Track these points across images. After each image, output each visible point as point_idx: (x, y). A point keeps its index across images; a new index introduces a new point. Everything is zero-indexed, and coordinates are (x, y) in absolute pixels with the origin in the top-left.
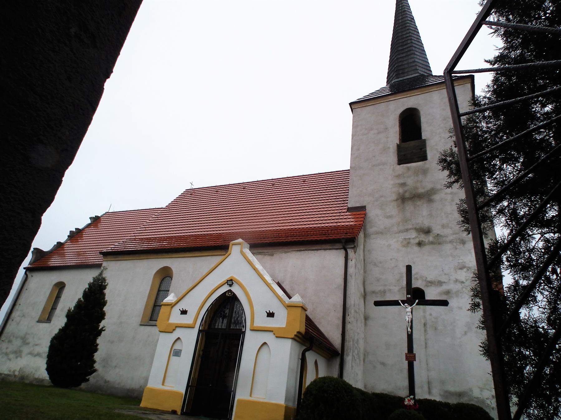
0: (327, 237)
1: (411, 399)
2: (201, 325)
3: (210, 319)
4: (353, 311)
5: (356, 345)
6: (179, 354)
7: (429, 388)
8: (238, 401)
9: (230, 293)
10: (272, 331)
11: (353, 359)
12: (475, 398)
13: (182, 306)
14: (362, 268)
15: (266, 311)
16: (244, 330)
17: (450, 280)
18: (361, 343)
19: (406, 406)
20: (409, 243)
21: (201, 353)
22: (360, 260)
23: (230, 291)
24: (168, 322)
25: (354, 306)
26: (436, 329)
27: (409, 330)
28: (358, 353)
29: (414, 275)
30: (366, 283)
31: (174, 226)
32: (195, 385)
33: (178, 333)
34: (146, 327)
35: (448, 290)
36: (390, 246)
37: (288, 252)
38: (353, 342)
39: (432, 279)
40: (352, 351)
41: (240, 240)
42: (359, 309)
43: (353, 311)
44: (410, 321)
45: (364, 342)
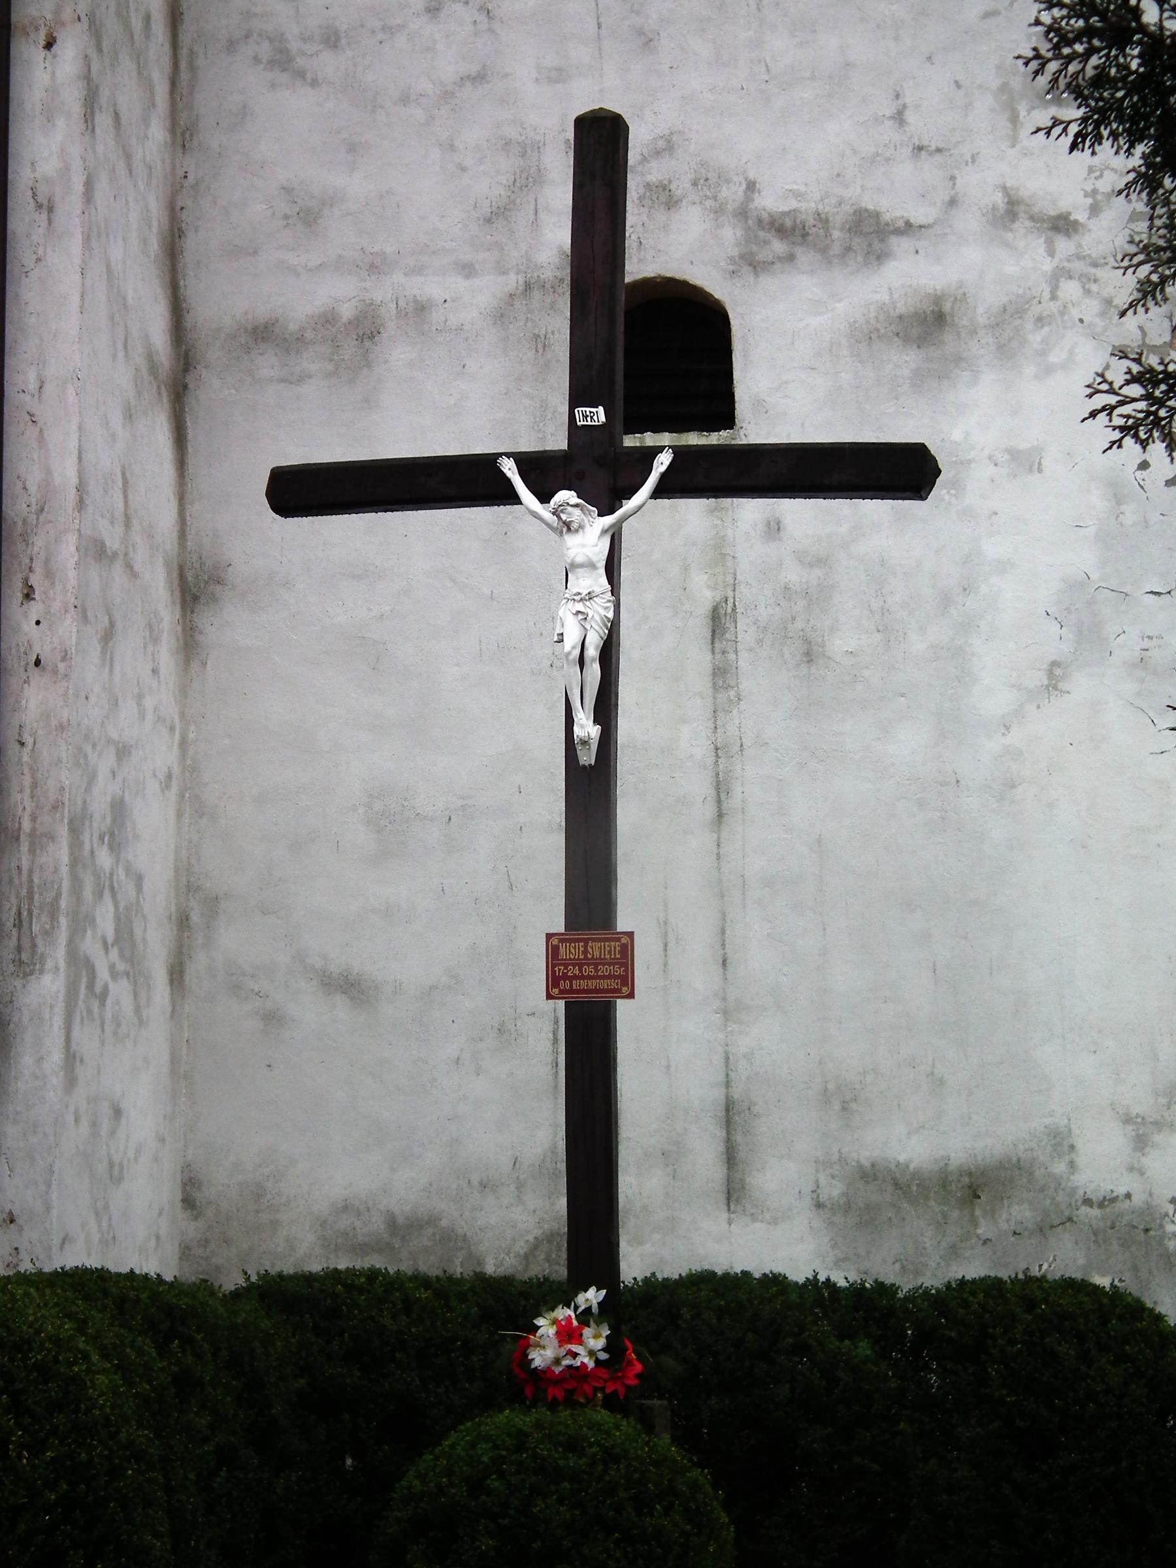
1: (585, 1316)
4: (68, 552)
5: (104, 859)
7: (731, 1157)
11: (83, 991)
12: (1088, 1202)
17: (953, 202)
22: (137, 23)
25: (81, 504)
26: (811, 654)
27: (587, 728)
29: (644, 160)
30: (191, 244)
35: (938, 299)
38: (76, 843)
39: (797, 195)
40: (63, 921)
42: (128, 524)
44: (592, 652)
45: (179, 815)
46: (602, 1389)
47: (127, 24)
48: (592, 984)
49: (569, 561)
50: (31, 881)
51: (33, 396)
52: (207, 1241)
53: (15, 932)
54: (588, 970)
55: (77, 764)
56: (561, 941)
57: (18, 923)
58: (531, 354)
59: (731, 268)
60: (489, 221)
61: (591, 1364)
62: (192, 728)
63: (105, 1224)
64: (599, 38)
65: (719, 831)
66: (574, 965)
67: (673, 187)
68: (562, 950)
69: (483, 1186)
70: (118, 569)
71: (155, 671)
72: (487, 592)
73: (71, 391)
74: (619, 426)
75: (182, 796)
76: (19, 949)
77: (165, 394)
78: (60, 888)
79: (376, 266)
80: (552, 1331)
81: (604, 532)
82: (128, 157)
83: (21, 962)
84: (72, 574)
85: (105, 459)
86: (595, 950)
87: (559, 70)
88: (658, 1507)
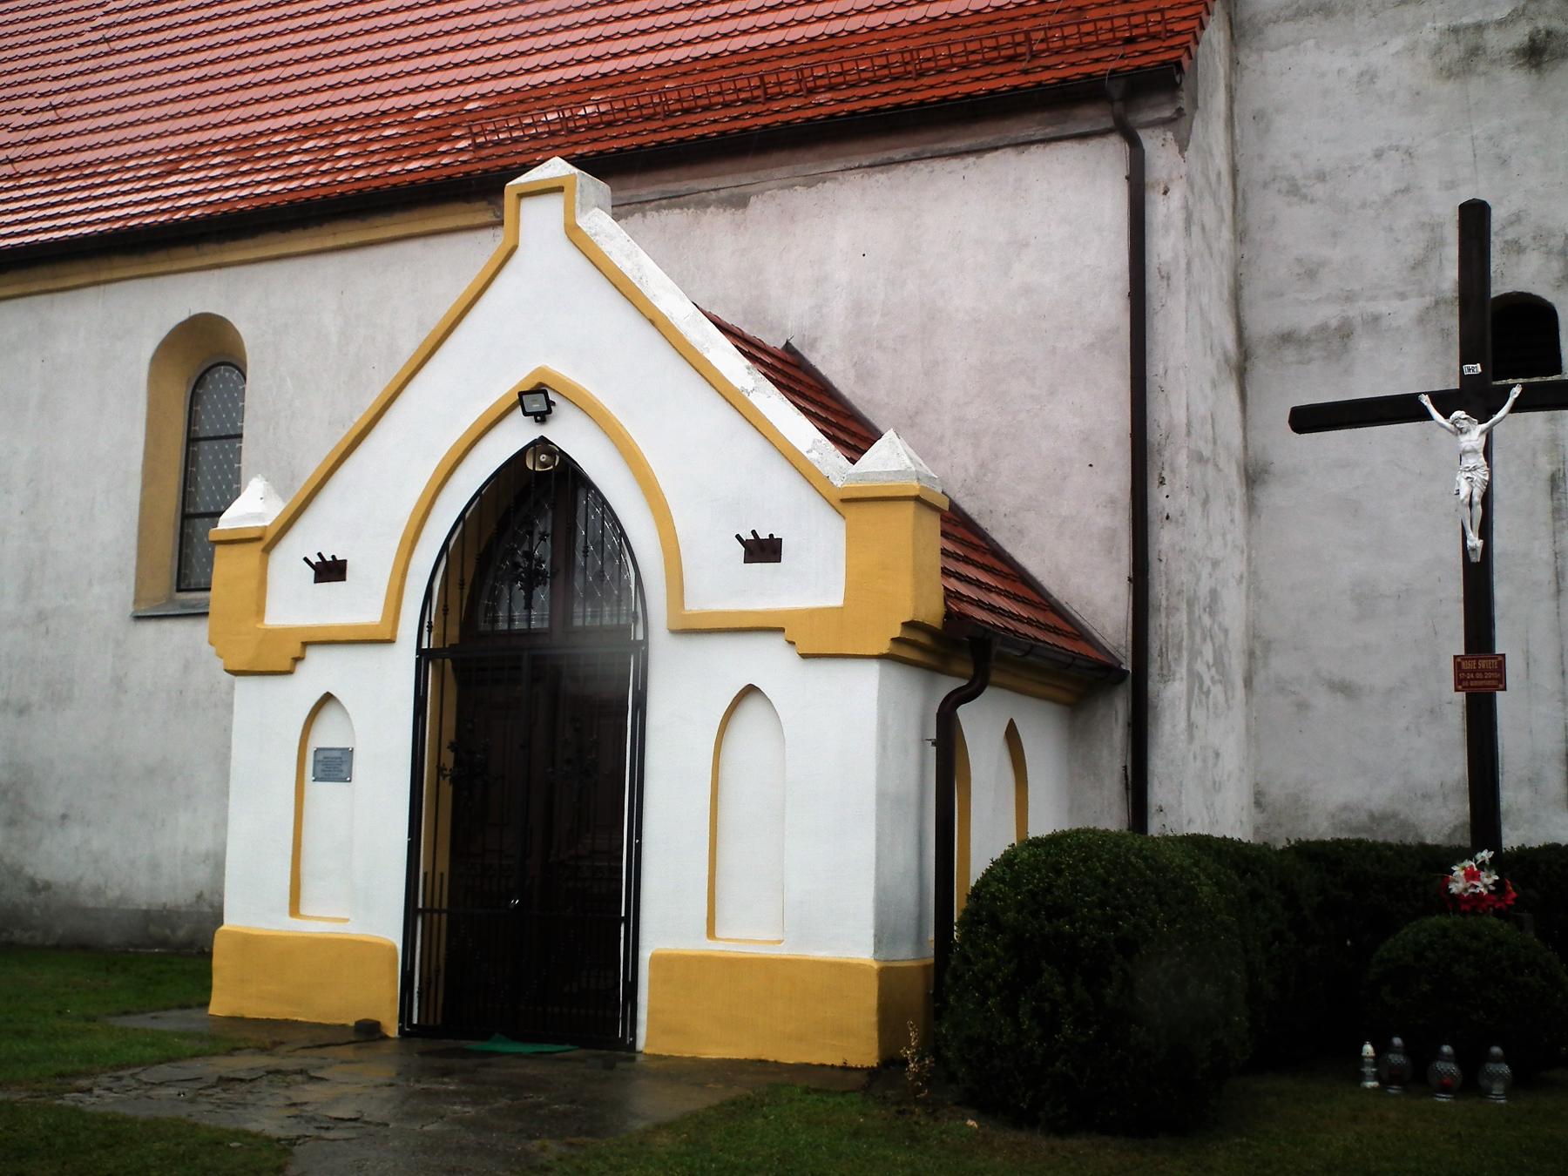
0: (1025, 72)
1: (1482, 866)
2: (426, 629)
3: (467, 591)
4: (1182, 459)
5: (1207, 620)
6: (344, 768)
8: (656, 960)
9: (543, 458)
10: (782, 630)
13: (311, 539)
14: (1222, 220)
15: (738, 537)
16: (640, 637)
18: (1234, 609)
19: (1457, 898)
20: (1475, 52)
21: (449, 759)
22: (1213, 178)
23: (542, 444)
24: (259, 626)
25: (1189, 433)
27: (1475, 541)
28: (1215, 659)
30: (1246, 293)
31: (199, 80)
32: (445, 906)
33: (320, 671)
34: (167, 625)
36: (1372, 81)
37: (823, 178)
38: (1190, 612)
40: (1185, 654)
41: (556, 168)
42: (1215, 443)
43: (1182, 459)
44: (1477, 499)
45: (1248, 597)
46: (1493, 906)
47: (1207, 178)
48: (1481, 683)
49: (1462, 449)
50: (1167, 632)
51: (1161, 377)
52: (1269, 824)
53: (1159, 658)
54: (1479, 675)
55: (1190, 570)
56: (1465, 659)
57: (1161, 655)
58: (1440, 340)
59: (1558, 284)
60: (1413, 268)
61: (1485, 892)
62: (1253, 551)
63: (1211, 813)
64: (1475, 162)
65: (1558, 600)
66: (1470, 673)
67: (1521, 241)
68: (1463, 663)
69: (1424, 796)
70: (1210, 467)
71: (1232, 521)
72: (1418, 471)
73: (1182, 373)
74: (1490, 375)
75: (1249, 587)
76: (1162, 668)
77: (1234, 374)
78: (1182, 636)
79: (1350, 298)
80: (1462, 873)
81: (1482, 432)
82: (1210, 247)
83: (1163, 675)
84: (1185, 470)
85: (1201, 409)
86: (1483, 664)
87: (1452, 182)
88: (1526, 971)
